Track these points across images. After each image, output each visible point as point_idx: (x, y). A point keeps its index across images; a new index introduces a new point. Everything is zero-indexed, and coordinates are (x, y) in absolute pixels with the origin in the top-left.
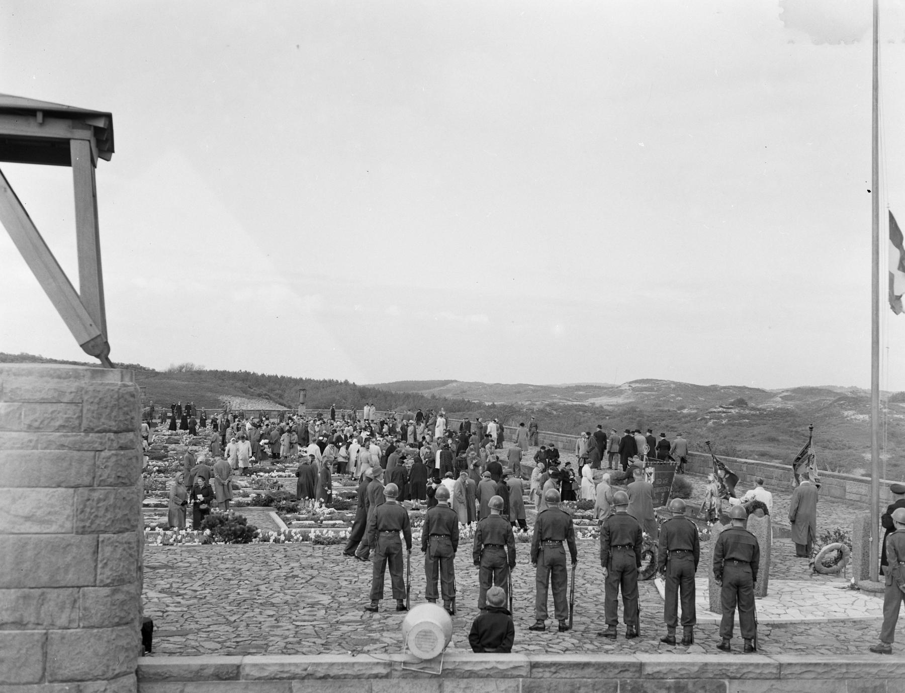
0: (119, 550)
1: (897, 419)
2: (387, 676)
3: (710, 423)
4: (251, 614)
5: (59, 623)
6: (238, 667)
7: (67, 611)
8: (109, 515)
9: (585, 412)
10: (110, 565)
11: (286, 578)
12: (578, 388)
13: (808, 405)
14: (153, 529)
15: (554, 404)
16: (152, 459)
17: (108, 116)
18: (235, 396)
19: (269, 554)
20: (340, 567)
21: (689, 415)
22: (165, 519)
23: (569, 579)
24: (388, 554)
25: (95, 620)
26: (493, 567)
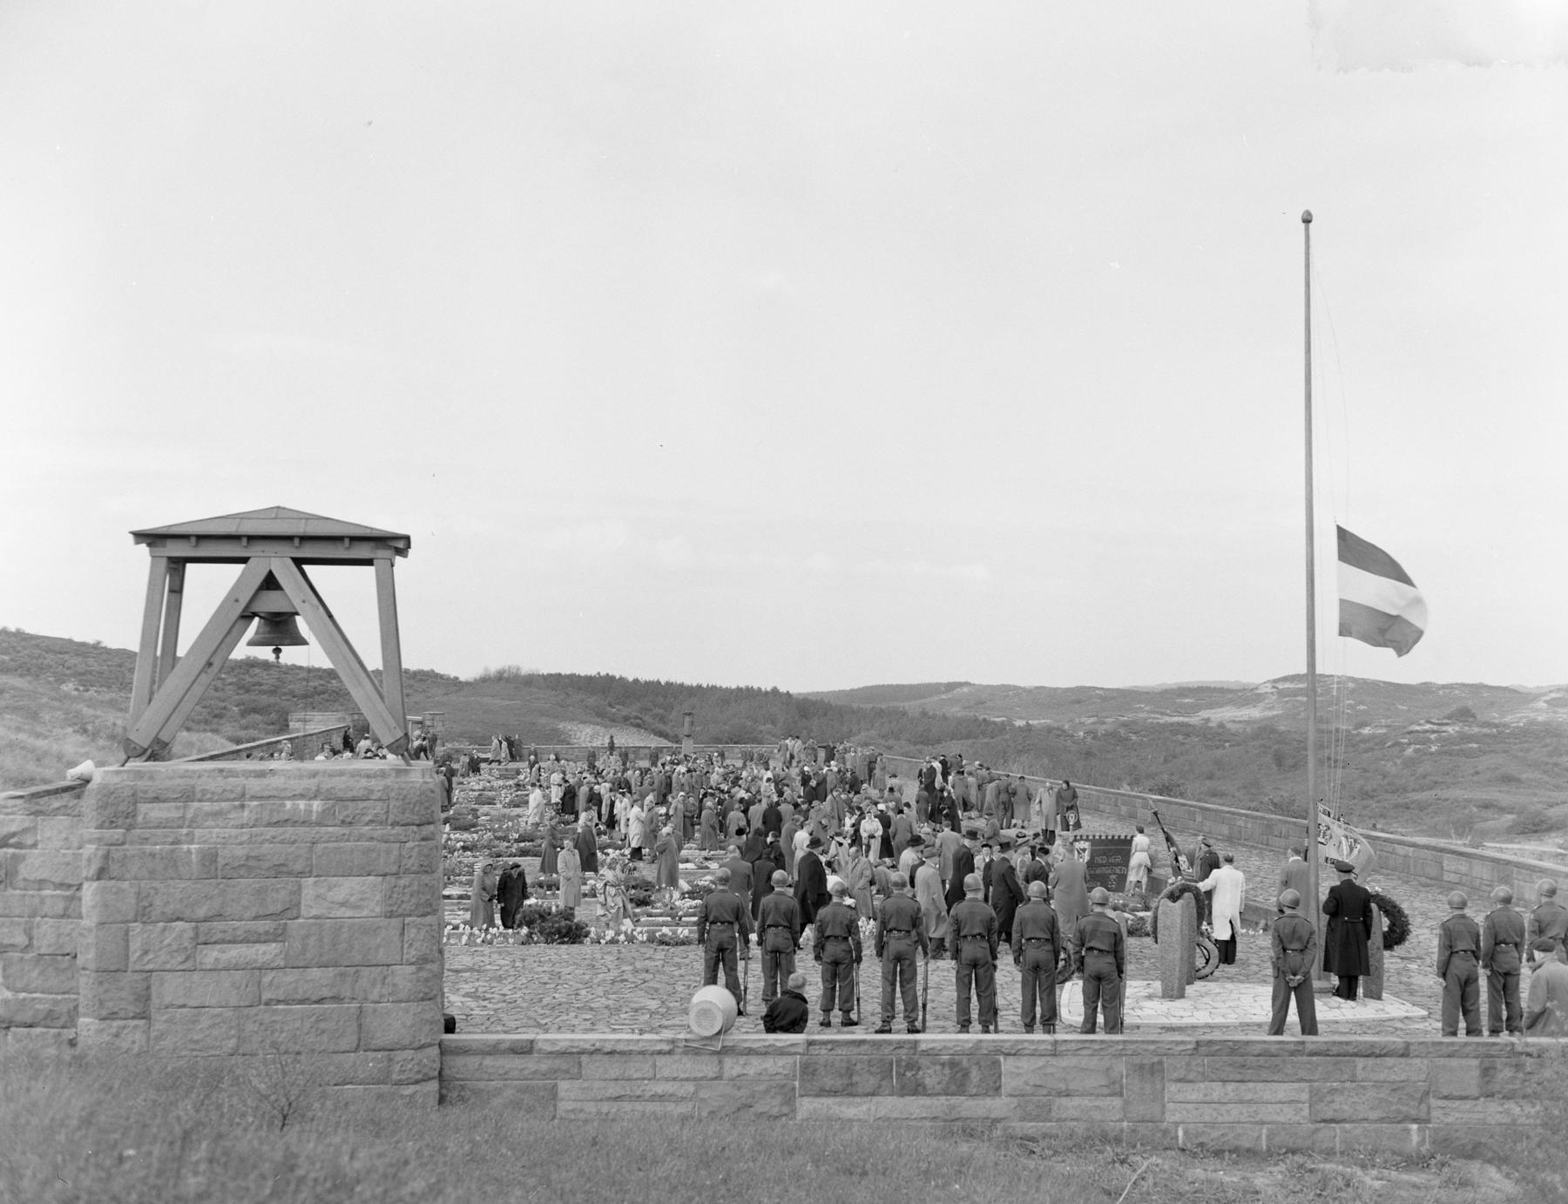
0: (423, 932)
2: (670, 1052)
3: (1409, 751)
4: (564, 1017)
5: (371, 997)
6: (532, 1042)
7: (378, 987)
8: (414, 900)
10: (417, 945)
11: (613, 982)
12: (1183, 691)
14: (456, 928)
15: (1135, 722)
16: (455, 829)
17: (407, 539)
18: (584, 722)
19: (598, 956)
20: (682, 972)
21: (1373, 737)
22: (468, 916)
23: (920, 978)
24: (721, 950)
25: (402, 995)
26: (836, 963)
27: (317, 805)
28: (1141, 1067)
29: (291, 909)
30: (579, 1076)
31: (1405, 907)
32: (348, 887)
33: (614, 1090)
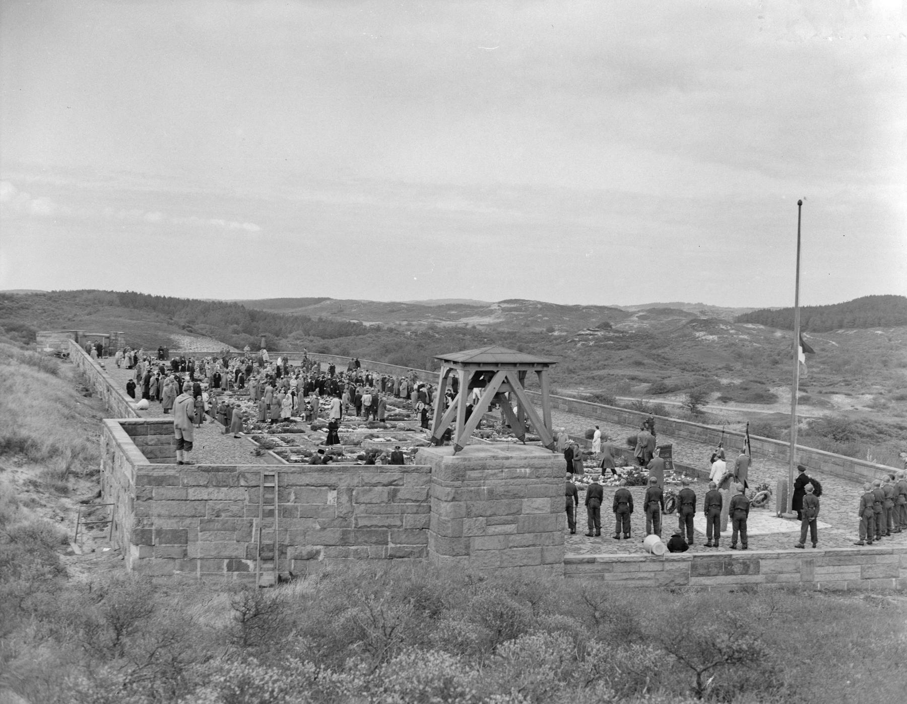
1: (742, 340)
3: (579, 345)
9: (464, 334)
12: (450, 307)
13: (662, 324)
21: (560, 337)
27: (528, 470)
28: (807, 562)
29: (519, 512)
30: (612, 571)
31: (821, 483)
32: (539, 502)
33: (625, 576)
